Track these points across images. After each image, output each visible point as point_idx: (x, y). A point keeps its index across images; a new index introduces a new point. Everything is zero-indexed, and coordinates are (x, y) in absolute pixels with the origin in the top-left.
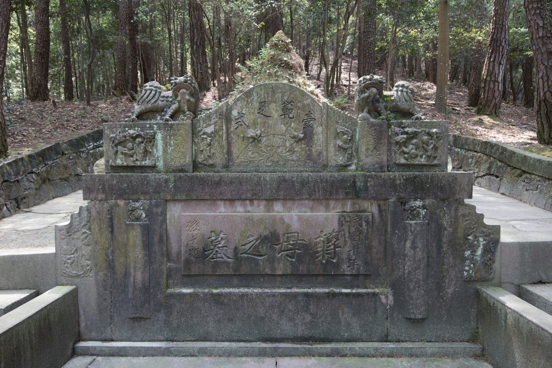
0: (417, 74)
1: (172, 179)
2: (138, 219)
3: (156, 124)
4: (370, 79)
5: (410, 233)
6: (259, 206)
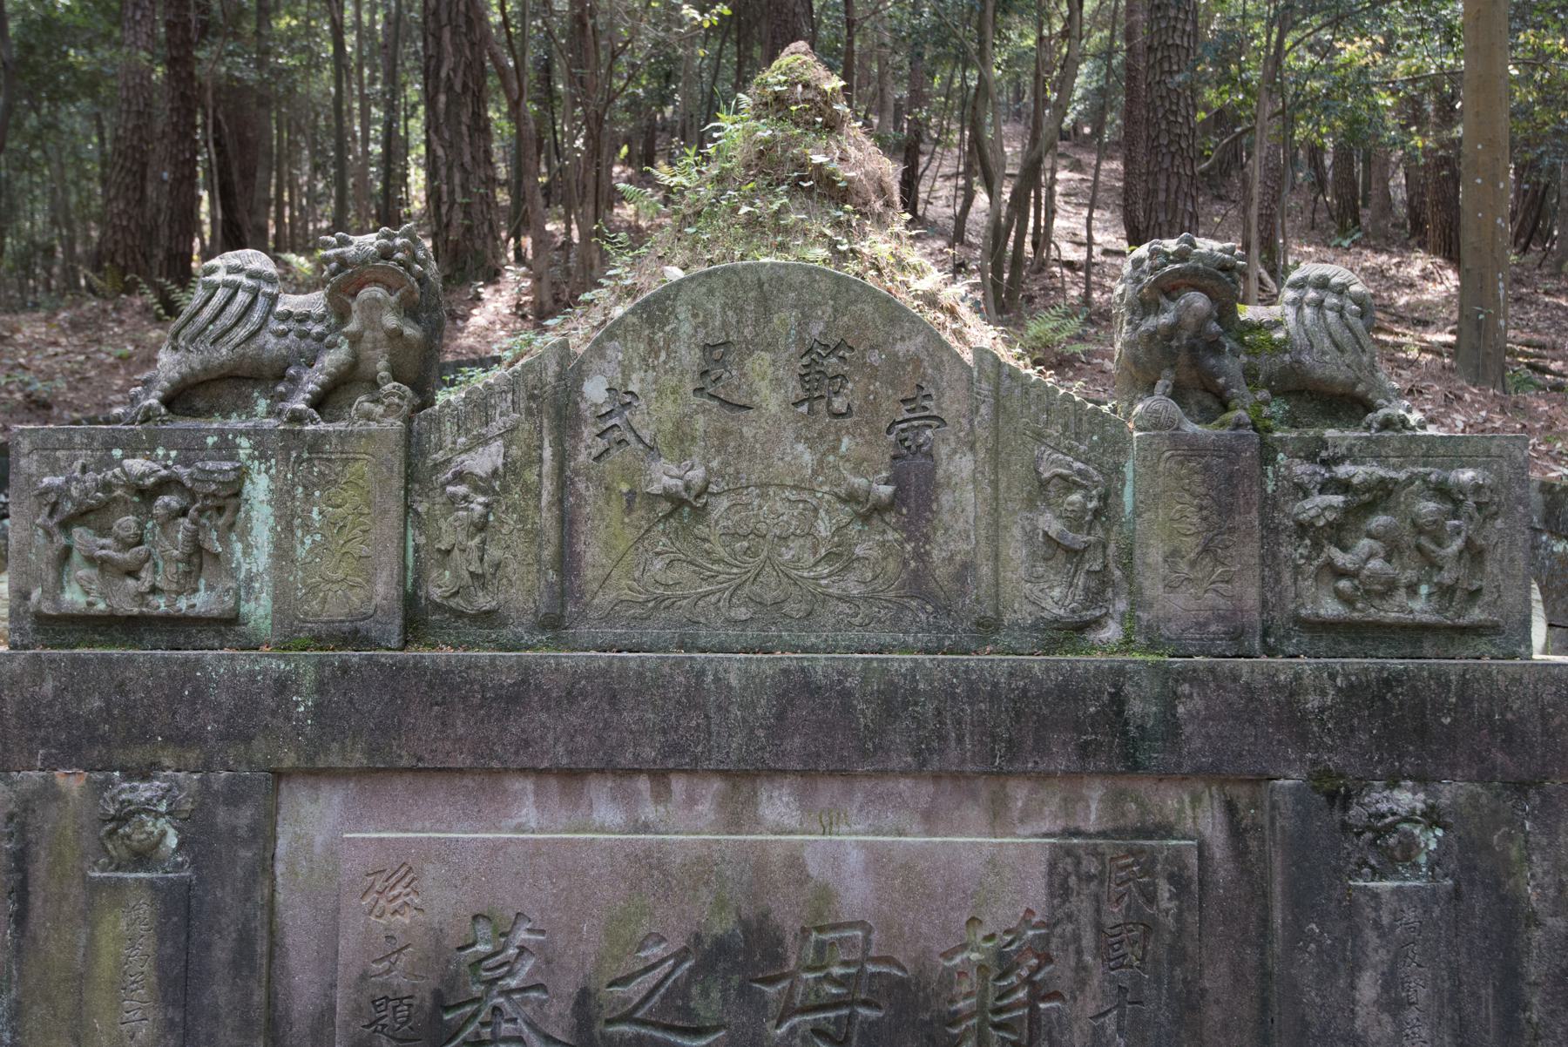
0: (1374, 221)
1: (309, 678)
2: (143, 857)
3: (246, 434)
4: (1181, 256)
5: (1371, 936)
6: (691, 801)
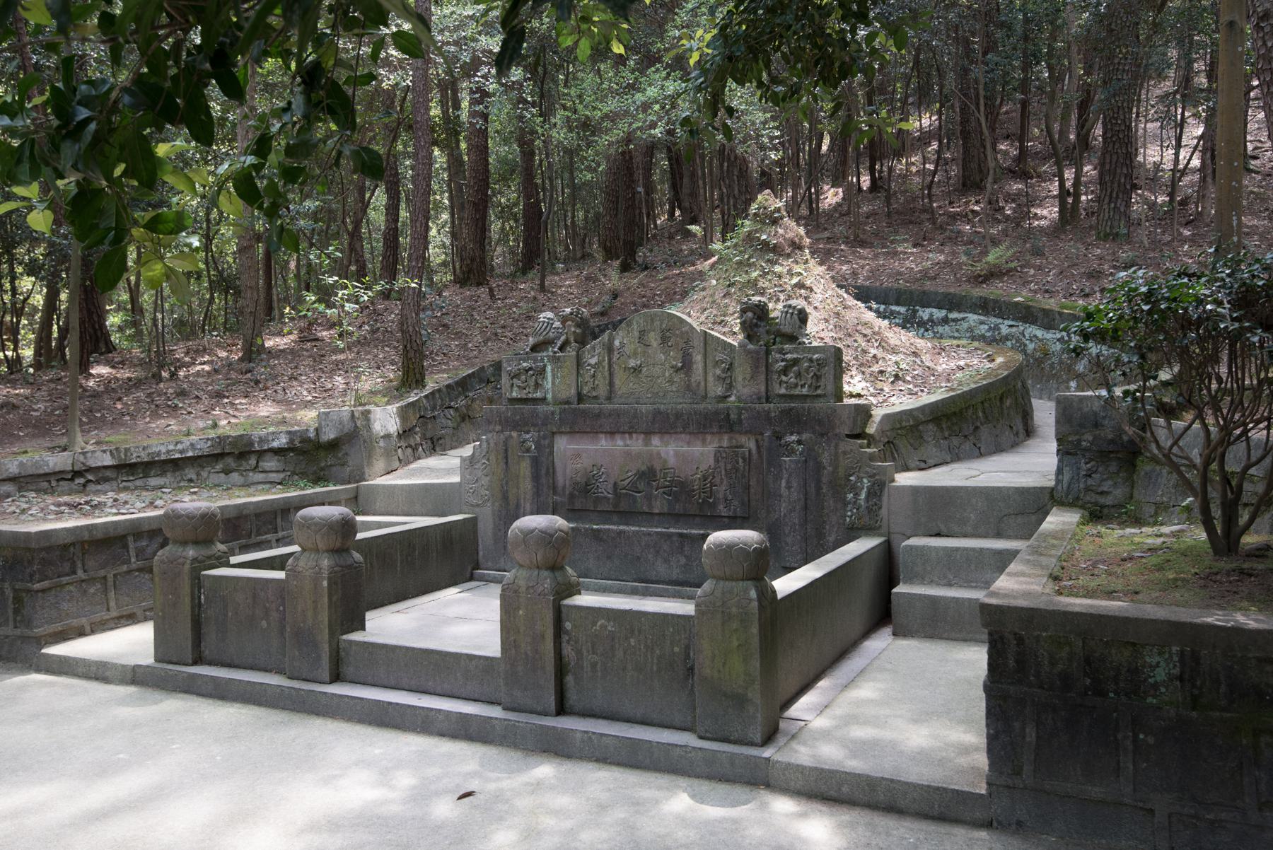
2: (528, 450)
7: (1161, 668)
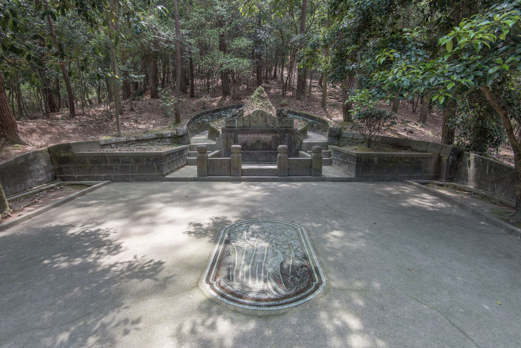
7: (376, 159)
